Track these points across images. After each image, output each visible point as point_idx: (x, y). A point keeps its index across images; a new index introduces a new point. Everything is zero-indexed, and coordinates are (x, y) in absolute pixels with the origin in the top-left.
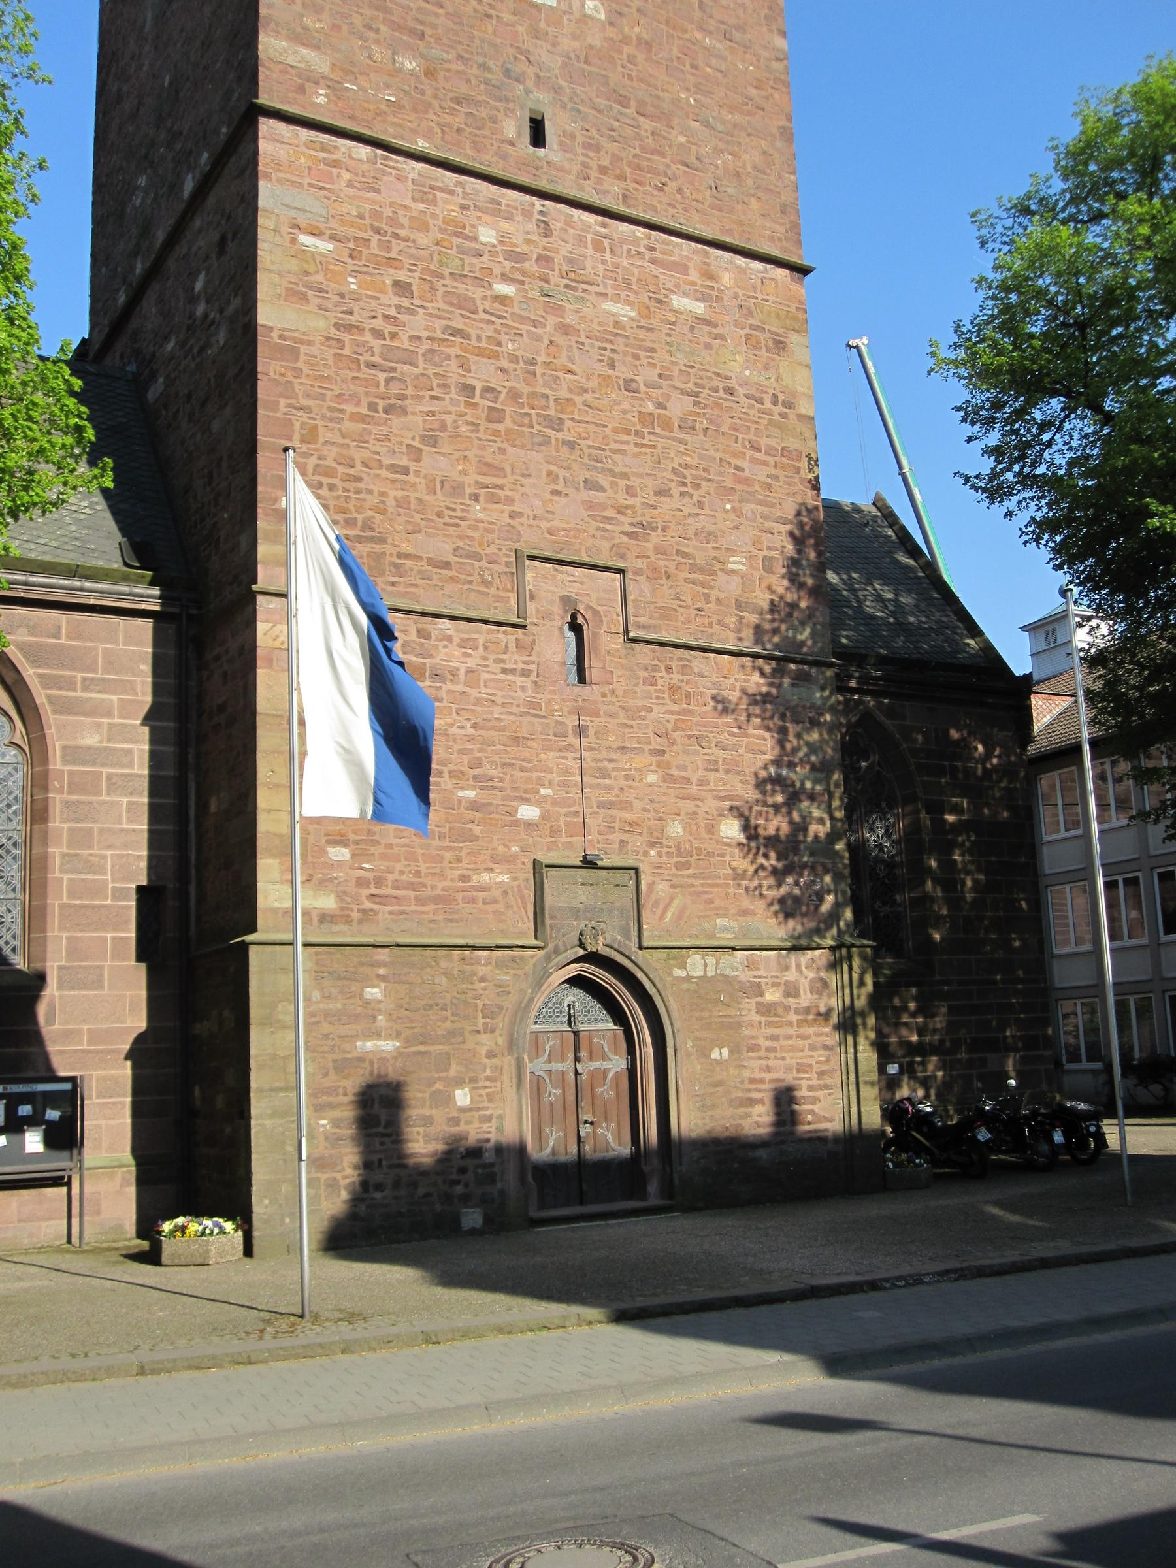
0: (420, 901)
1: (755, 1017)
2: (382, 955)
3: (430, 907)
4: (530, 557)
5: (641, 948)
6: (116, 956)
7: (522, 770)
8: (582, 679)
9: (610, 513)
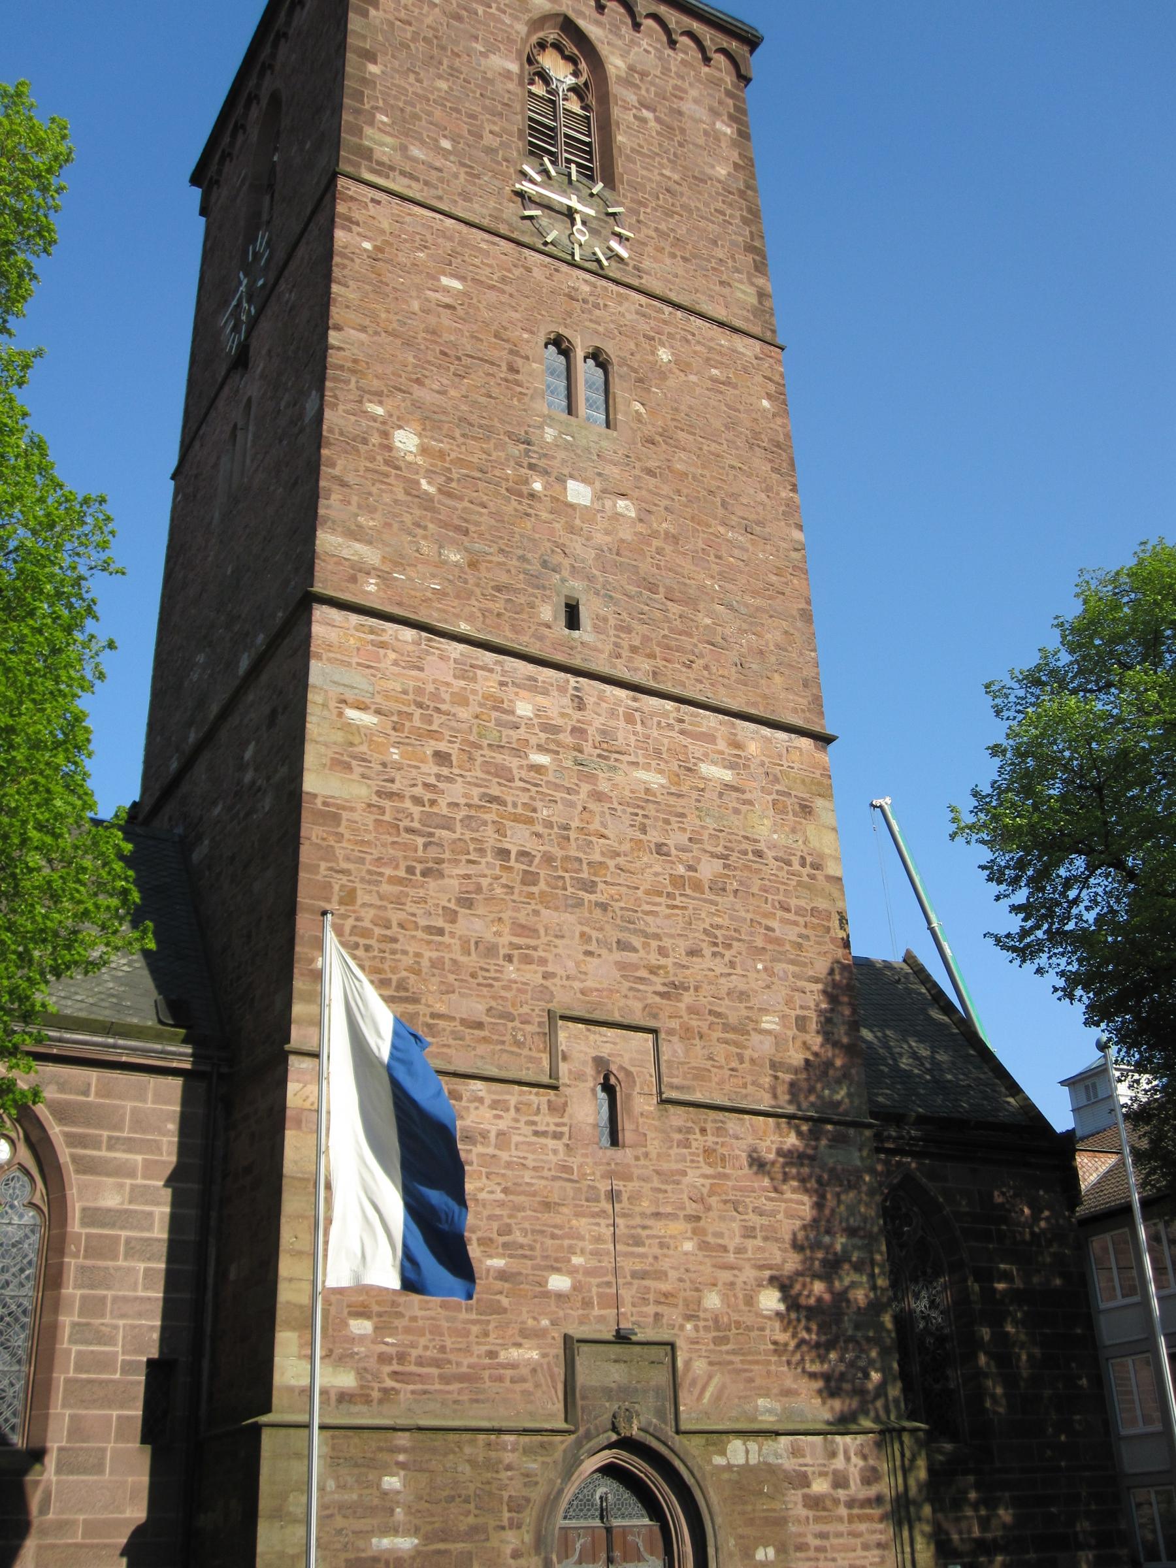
1: (802, 1512)
2: (403, 1439)
4: (563, 1018)
5: (678, 1432)
6: (120, 1437)
7: (553, 1237)
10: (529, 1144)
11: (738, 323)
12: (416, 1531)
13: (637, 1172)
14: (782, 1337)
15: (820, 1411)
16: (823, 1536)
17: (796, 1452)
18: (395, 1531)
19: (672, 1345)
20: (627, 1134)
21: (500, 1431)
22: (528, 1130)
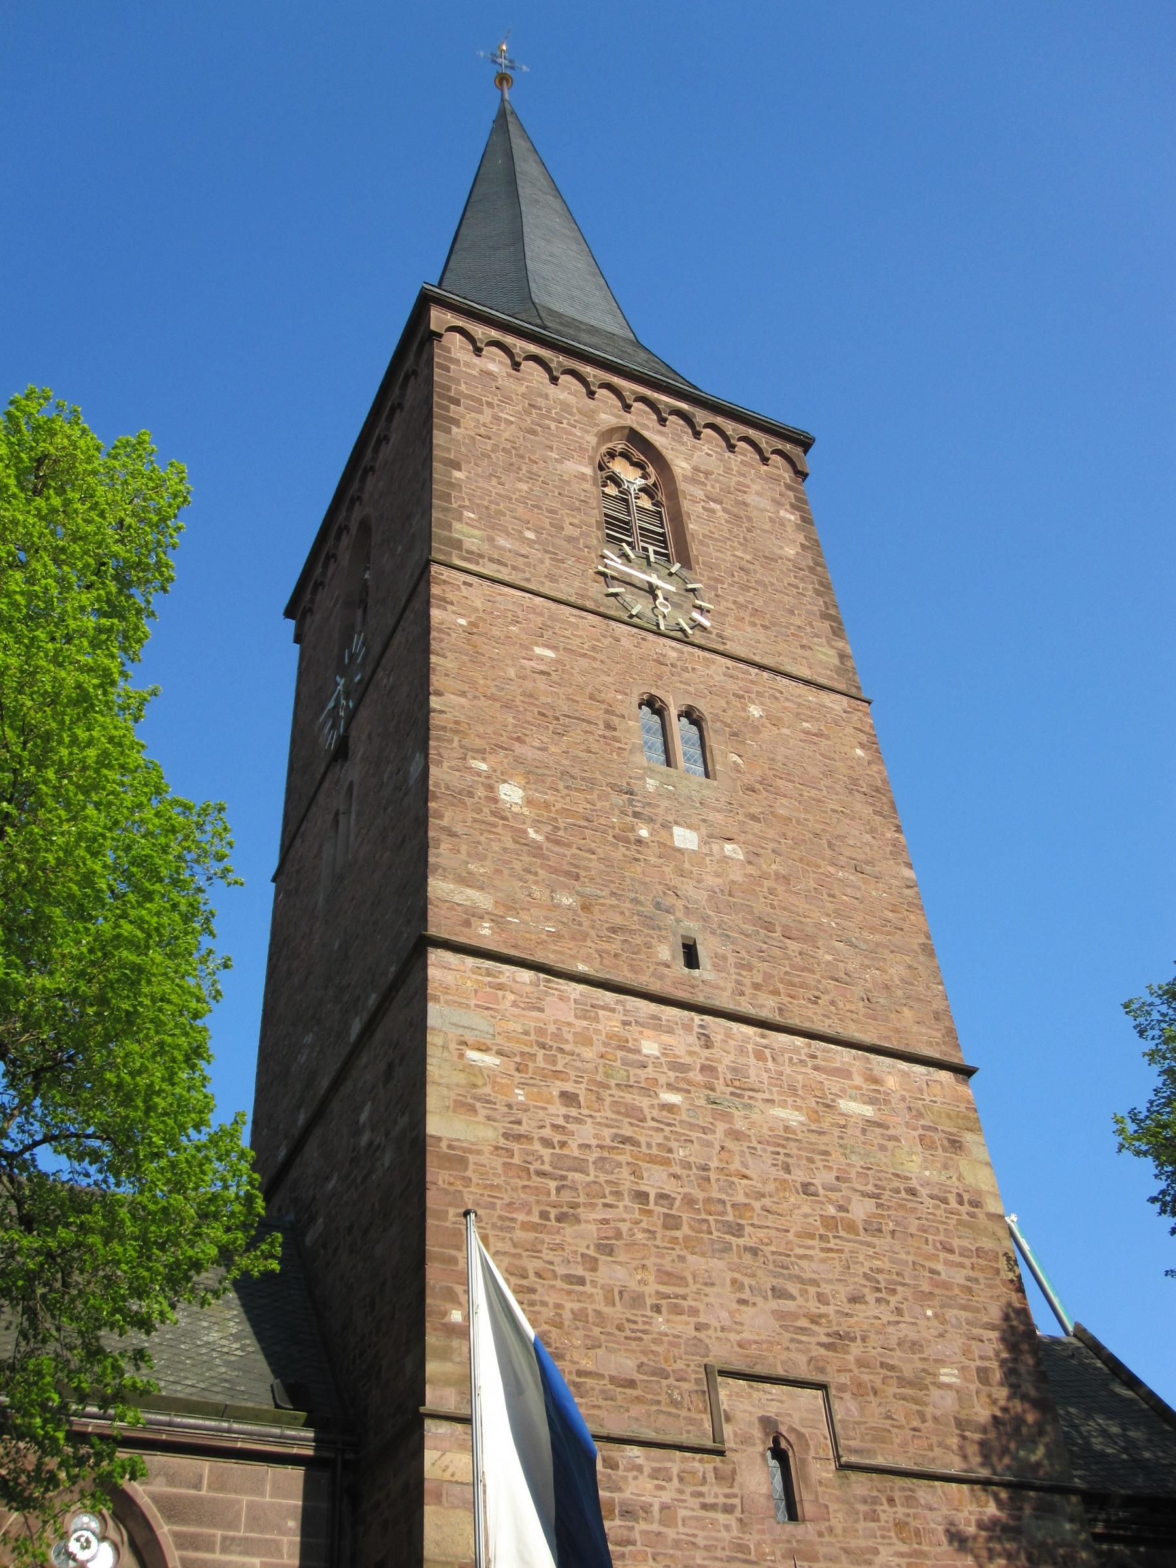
4: (722, 1373)
9: (803, 1323)
10: (697, 1519)
13: (822, 1550)
20: (807, 1507)
22: (694, 1502)
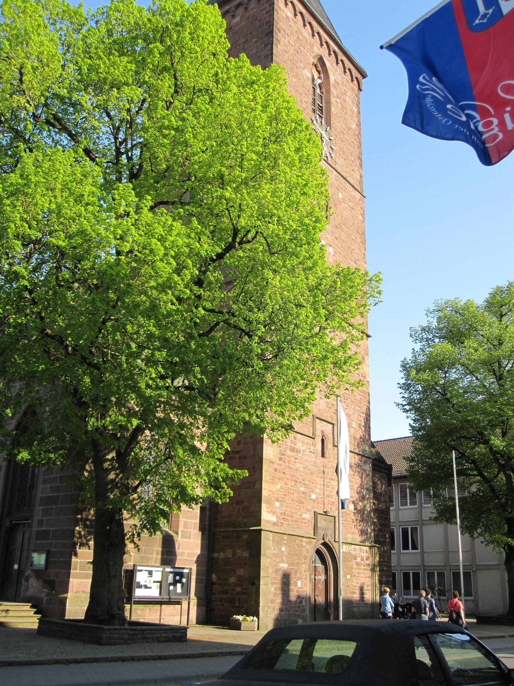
0: (292, 521)
1: (355, 566)
2: (285, 537)
3: (294, 523)
4: (317, 418)
5: (335, 541)
6: (195, 529)
8: (323, 456)
9: (330, 406)
11: (355, 186)
12: (287, 563)
14: (353, 517)
15: (358, 539)
16: (358, 573)
17: (355, 550)
18: (283, 562)
19: (335, 517)
20: (327, 455)
21: (303, 537)
22: (308, 450)
